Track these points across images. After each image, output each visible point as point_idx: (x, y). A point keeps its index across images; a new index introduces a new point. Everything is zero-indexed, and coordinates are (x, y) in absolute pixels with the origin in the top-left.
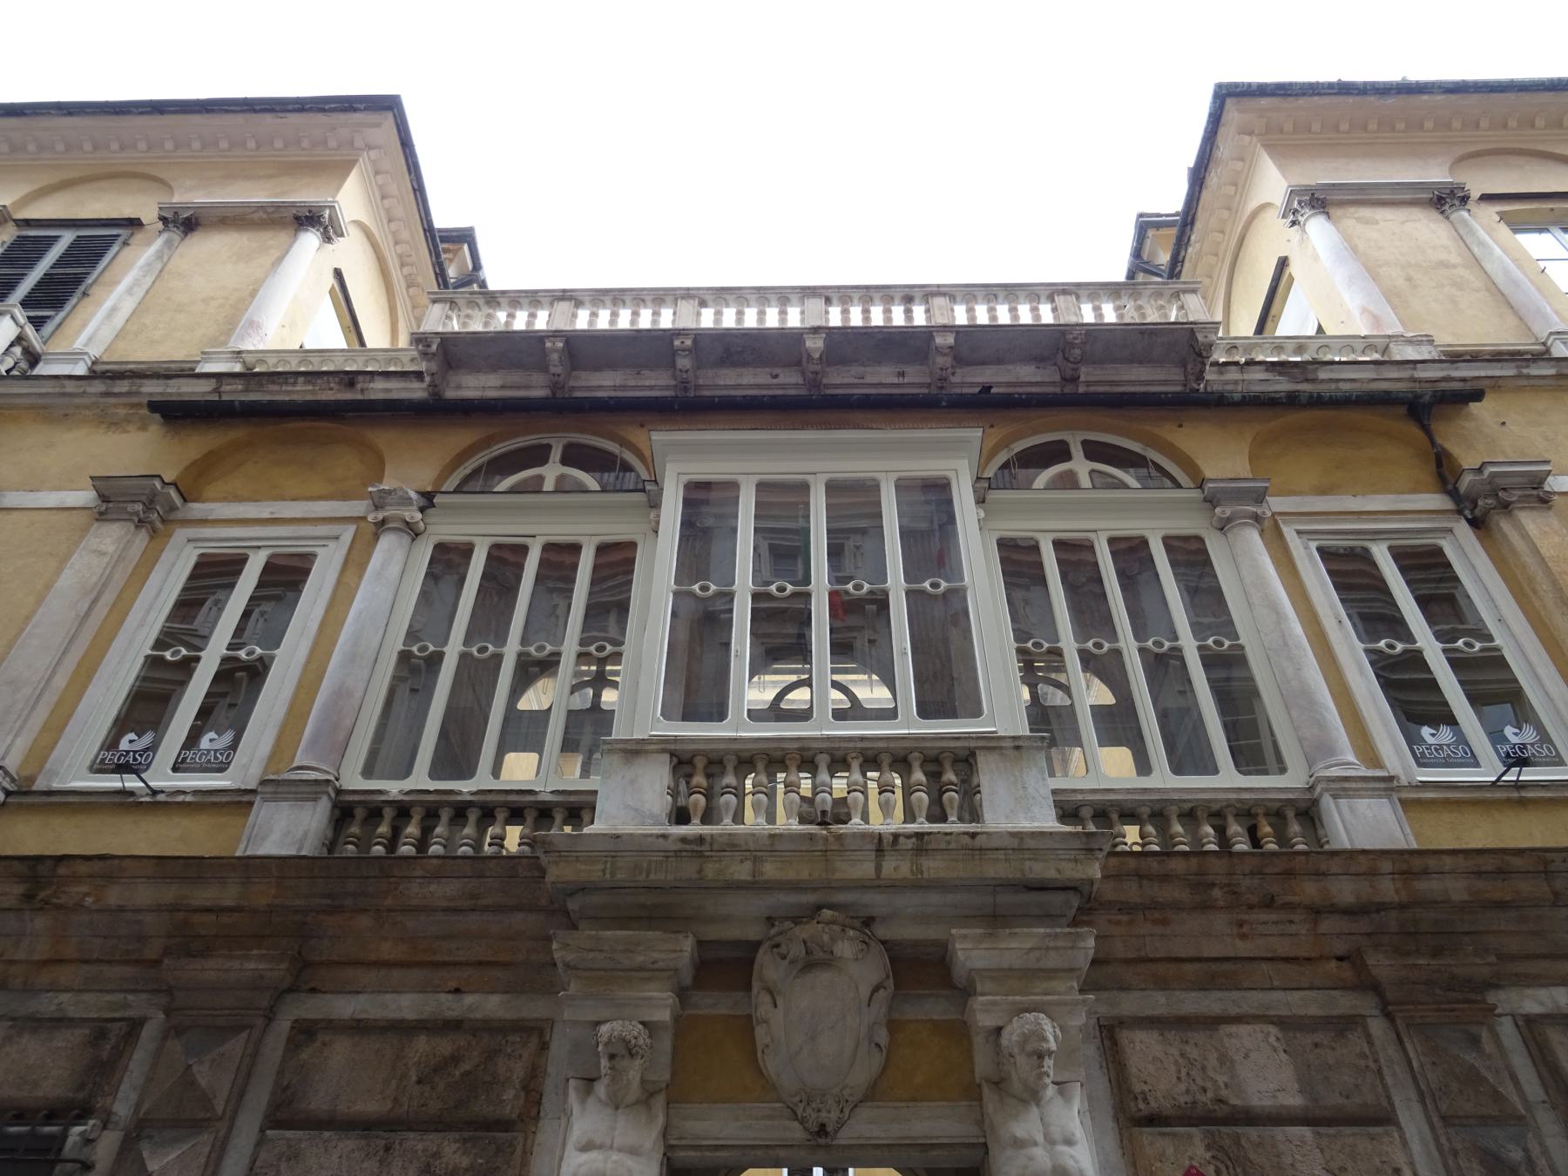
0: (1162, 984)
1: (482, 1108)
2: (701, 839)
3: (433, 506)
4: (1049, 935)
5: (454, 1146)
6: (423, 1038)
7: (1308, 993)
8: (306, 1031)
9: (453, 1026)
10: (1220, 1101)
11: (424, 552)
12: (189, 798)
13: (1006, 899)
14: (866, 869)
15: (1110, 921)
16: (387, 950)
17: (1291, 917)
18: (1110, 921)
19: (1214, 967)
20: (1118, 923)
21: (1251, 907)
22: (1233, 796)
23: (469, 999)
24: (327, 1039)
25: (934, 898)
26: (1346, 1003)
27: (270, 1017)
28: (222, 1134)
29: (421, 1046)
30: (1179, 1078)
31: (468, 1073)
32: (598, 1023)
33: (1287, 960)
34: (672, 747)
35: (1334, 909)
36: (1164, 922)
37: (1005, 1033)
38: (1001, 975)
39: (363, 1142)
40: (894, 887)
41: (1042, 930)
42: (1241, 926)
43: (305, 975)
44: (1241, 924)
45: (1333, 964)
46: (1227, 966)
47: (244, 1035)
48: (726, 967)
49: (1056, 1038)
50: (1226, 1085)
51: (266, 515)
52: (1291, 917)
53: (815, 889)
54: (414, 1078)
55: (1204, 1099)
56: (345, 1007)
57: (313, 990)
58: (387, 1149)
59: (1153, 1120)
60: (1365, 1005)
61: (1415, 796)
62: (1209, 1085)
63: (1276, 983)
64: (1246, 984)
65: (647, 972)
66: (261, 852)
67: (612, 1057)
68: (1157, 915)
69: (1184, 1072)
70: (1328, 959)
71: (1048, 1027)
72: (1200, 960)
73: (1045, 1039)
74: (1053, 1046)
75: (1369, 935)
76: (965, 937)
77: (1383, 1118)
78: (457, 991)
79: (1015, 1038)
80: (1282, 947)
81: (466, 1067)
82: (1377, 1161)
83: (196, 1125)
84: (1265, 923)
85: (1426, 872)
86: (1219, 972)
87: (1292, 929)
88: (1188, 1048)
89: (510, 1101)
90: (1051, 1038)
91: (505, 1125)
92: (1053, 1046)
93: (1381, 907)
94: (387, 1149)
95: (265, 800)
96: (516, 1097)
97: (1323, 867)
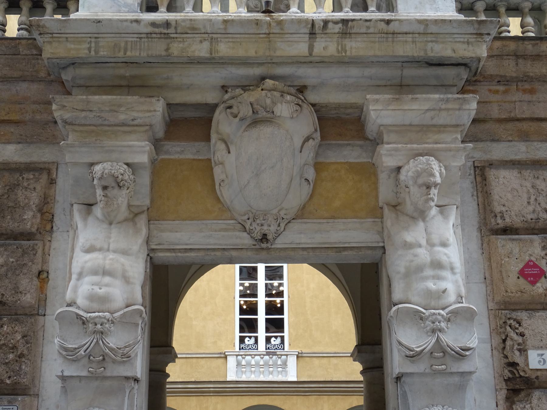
0: (525, 137)
2: (167, 24)
4: (442, 100)
13: (411, 72)
14: (301, 48)
18: (490, 91)
25: (354, 71)
30: (529, 203)
32: (92, 164)
36: (532, 91)
37: (403, 171)
38: (403, 130)
41: (437, 96)
48: (191, 123)
49: (441, 174)
67: (105, 188)
68: (527, 86)
71: (436, 166)
73: (433, 175)
74: (438, 180)
76: (377, 101)
79: (410, 174)
88: (538, 182)
89: (30, 220)
90: (437, 174)
91: (29, 236)
92: (438, 180)
96: (34, 216)
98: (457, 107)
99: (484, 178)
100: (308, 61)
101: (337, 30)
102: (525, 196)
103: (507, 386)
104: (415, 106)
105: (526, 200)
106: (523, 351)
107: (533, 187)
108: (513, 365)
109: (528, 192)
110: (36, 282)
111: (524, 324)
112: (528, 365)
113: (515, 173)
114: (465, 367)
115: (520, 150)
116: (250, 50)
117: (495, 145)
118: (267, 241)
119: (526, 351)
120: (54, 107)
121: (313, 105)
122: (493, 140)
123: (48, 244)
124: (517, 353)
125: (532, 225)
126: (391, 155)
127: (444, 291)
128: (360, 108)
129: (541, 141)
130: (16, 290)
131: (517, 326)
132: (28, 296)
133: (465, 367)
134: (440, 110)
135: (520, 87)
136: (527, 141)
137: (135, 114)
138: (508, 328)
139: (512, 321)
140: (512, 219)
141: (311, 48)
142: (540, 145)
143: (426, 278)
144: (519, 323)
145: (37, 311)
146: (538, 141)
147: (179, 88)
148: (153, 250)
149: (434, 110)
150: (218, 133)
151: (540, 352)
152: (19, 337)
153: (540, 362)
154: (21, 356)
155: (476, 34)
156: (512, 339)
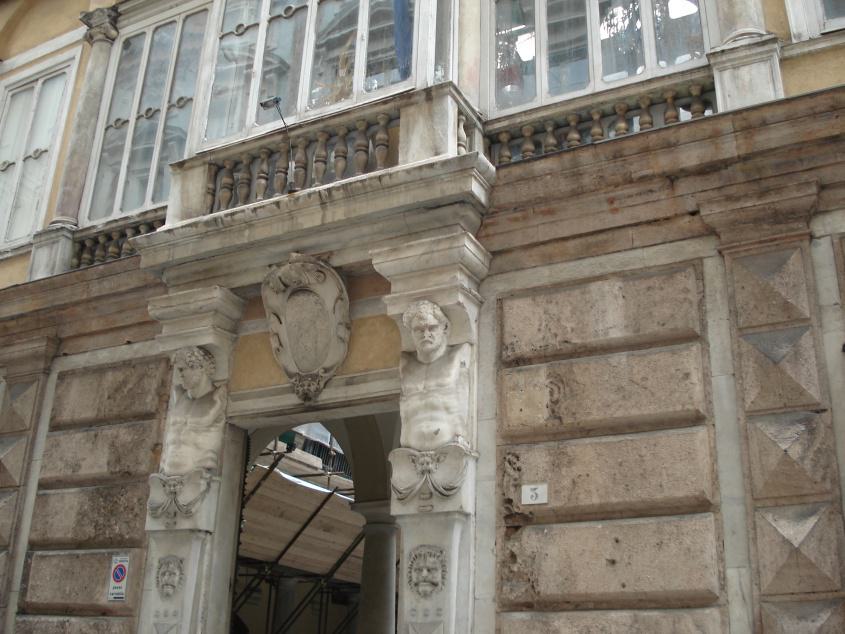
0: (548, 260)
1: (138, 408)
3: (120, 15)
4: (434, 242)
5: (124, 431)
6: (110, 373)
7: (660, 247)
8: (62, 376)
9: (127, 364)
10: (566, 342)
11: (118, 47)
12: (9, 255)
13: (412, 219)
15: (510, 220)
16: (95, 326)
17: (650, 187)
18: (510, 220)
19: (591, 239)
20: (516, 220)
21: (617, 185)
22: (643, 89)
23: (136, 346)
24: (69, 380)
25: (366, 230)
26: (691, 249)
27: (47, 372)
28: (31, 437)
29: (110, 378)
30: (539, 330)
31: (131, 389)
33: (649, 223)
34: (208, 159)
35: (686, 173)
36: (550, 212)
38: (408, 275)
39: (85, 433)
40: (338, 227)
41: (428, 240)
42: (612, 202)
43: (59, 346)
44: (611, 201)
45: (687, 219)
46: (601, 237)
47: (35, 384)
48: (250, 301)
50: (572, 330)
51: (53, 49)
52: (650, 187)
53: (291, 240)
54: (106, 397)
55: (553, 342)
56: (78, 361)
57: (65, 355)
58: (96, 436)
59: (519, 362)
60: (704, 248)
61: (806, 49)
62: (560, 332)
63: (637, 244)
64: (611, 249)
65: (199, 313)
66: (36, 278)
68: (543, 208)
69: (544, 324)
70: (683, 215)
72: (580, 236)
75: (719, 188)
76: (378, 254)
77: (692, 337)
78: (129, 343)
80: (645, 213)
81: (130, 386)
82: (673, 370)
83: (21, 433)
84: (630, 196)
85: (764, 124)
86: (595, 241)
87: (654, 197)
88: (550, 306)
89: (150, 402)
91: (149, 416)
93: (726, 163)
94: (96, 436)
95: (37, 248)
96: (153, 399)
97: (673, 139)
98: (447, 246)
99: (501, 308)
100: (322, 229)
101: (341, 196)
102: (537, 323)
103: (506, 523)
104: (410, 253)
105: (536, 327)
106: (518, 486)
107: (545, 313)
108: (510, 501)
109: (540, 319)
110: (150, 453)
111: (522, 459)
112: (520, 501)
113: (529, 301)
114: (449, 506)
115: (543, 275)
116: (277, 230)
117: (519, 274)
118: (310, 399)
119: (520, 486)
120: (149, 308)
121: (336, 268)
122: (517, 270)
123: (163, 421)
124: (512, 489)
125: (542, 353)
126: (394, 304)
127: (436, 433)
128: (369, 263)
129: (566, 261)
130: (138, 463)
131: (515, 460)
132: (144, 466)
133: (449, 506)
134: (433, 252)
135: (536, 209)
136: (550, 264)
137: (200, 304)
138: (507, 464)
139: (510, 456)
140: (524, 349)
141: (324, 217)
142: (565, 265)
143: (420, 421)
144: (518, 458)
145: (144, 478)
146: (562, 262)
147: (238, 274)
148: (231, 417)
149: (427, 253)
150: (269, 307)
151: (533, 486)
152: (135, 500)
153: (532, 496)
154: (136, 515)
155: (461, 170)
156: (509, 475)
